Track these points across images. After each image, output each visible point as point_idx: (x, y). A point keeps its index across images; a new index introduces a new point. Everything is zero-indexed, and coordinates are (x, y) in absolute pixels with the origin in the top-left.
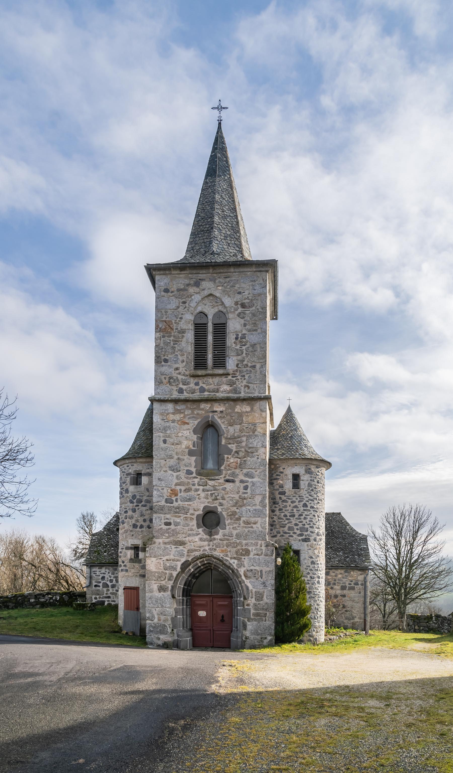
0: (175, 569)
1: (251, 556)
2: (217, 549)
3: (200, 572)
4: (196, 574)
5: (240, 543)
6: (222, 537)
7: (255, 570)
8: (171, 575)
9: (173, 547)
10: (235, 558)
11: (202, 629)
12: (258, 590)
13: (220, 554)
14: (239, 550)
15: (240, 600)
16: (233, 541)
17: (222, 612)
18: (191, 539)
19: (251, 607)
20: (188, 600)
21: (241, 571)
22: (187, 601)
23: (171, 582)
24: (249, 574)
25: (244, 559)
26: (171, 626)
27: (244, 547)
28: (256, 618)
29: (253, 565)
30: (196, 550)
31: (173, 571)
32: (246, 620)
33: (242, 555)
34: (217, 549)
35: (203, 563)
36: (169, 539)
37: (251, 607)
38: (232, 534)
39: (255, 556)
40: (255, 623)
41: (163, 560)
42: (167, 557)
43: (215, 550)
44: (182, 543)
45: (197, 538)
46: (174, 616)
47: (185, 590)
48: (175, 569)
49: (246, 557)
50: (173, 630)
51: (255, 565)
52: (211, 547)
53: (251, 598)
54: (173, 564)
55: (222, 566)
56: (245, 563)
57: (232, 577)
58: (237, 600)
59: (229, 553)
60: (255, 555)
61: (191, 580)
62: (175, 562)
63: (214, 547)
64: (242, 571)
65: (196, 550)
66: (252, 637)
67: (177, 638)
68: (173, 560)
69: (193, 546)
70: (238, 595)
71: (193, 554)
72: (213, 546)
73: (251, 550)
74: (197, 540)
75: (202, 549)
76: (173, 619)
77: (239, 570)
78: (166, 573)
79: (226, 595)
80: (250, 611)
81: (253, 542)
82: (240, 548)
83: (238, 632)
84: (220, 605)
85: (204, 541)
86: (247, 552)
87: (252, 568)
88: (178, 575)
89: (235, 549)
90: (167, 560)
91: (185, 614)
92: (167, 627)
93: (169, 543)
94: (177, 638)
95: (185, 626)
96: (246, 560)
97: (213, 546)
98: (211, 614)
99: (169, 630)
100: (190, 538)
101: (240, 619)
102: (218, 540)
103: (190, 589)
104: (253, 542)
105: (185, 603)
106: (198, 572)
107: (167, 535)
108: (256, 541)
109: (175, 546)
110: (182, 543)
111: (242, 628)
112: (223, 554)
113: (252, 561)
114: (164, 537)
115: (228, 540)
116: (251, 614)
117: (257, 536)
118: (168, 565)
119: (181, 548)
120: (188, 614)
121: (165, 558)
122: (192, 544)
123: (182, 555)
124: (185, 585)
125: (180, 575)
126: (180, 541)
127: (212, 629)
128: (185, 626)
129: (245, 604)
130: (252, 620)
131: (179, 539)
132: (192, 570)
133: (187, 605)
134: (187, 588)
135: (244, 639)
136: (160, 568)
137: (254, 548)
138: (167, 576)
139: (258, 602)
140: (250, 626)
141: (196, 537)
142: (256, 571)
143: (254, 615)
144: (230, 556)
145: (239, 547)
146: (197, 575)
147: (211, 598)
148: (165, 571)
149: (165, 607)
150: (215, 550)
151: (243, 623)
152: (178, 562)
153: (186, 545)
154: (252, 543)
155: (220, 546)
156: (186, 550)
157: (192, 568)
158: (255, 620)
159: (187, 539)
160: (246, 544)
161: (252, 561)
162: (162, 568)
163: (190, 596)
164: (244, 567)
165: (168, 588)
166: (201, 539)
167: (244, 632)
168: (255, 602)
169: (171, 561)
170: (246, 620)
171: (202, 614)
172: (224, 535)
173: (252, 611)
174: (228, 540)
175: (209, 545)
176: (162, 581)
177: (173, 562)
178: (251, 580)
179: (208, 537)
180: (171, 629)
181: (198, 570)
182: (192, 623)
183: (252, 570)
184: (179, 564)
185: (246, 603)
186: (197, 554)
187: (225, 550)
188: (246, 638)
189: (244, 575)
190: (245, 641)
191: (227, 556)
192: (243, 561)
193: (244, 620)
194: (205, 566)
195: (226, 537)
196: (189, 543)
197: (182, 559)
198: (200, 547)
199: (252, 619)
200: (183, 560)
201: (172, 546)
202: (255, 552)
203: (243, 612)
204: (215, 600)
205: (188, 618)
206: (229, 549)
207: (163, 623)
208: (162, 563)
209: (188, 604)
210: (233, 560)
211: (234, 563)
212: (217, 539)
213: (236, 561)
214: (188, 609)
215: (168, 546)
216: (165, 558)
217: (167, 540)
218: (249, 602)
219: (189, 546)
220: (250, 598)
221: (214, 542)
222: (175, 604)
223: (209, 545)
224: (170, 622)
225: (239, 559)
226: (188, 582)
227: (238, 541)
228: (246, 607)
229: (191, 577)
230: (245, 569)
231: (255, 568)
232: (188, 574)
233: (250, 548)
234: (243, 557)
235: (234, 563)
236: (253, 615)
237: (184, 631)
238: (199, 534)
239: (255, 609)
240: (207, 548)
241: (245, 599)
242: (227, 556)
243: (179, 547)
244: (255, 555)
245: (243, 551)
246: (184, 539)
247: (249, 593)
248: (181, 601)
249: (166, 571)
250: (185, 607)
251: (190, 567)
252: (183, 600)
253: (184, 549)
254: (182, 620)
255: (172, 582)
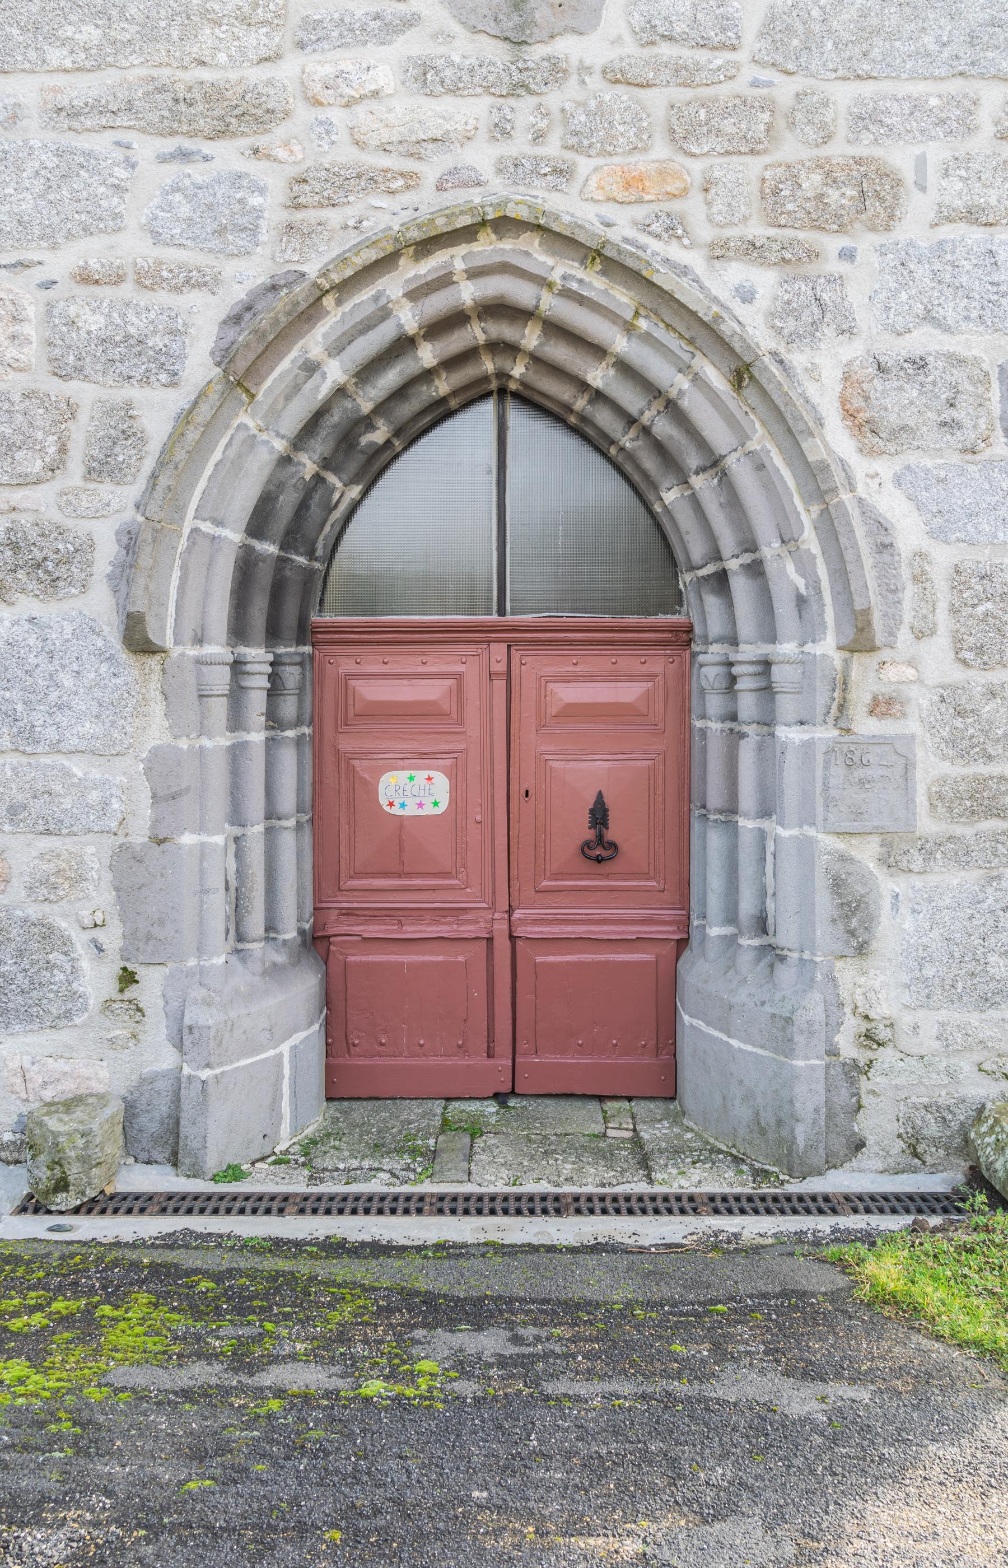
0: (166, 368)
1: (914, 226)
2: (584, 165)
3: (406, 410)
4: (367, 423)
5: (809, 110)
6: (630, 48)
7: (957, 361)
8: (123, 428)
9: (147, 148)
10: (752, 250)
11: (411, 931)
12: (983, 556)
13: (610, 211)
14: (792, 174)
15: (805, 663)
16: (741, 85)
17: (588, 772)
18: (329, 70)
19: (913, 726)
20: (291, 675)
21: (813, 371)
22: (274, 677)
23: (122, 499)
24: (896, 402)
25: (848, 255)
26: (112, 938)
27: (838, 150)
28: (968, 832)
29: (929, 317)
30: (371, 180)
31: (146, 381)
32: (866, 853)
33: (822, 218)
34: (584, 165)
35: (438, 304)
36: (110, 77)
37: (913, 726)
38: (726, 23)
39: (947, 232)
40: (954, 880)
41: (39, 275)
42: (90, 251)
43: (563, 172)
44: (243, 115)
45: (382, 66)
46: (139, 836)
47: (264, 576)
48: (166, 368)
49: (865, 243)
50: (128, 978)
51: (949, 313)
52: (519, 146)
53: (919, 635)
54: (143, 310)
55: (629, 329)
56: (856, 295)
57: (717, 434)
58: (766, 665)
59: (694, 208)
60: (946, 217)
61: (318, 479)
62: (163, 297)
63: (552, 148)
64: (819, 376)
65: (371, 180)
66: (929, 1021)
67: (166, 1059)
68: (149, 279)
69: (342, 136)
70: (784, 609)
71: (349, 214)
72: (539, 137)
73: (909, 176)
74: (384, 76)
75: (430, 172)
76: (135, 871)
77: (798, 359)
78: (72, 410)
79: (607, 619)
80: (908, 767)
81: (932, 93)
82: (806, 154)
83: (786, 974)
84: (573, 712)
85: (454, 91)
86: (875, 194)
87: (924, 340)
88: (185, 418)
89: (755, 165)
90: (86, 278)
91: (255, 804)
92: (66, 945)
93: (107, 112)
94: (166, 1059)
95: (256, 922)
96: (861, 272)
97: (539, 137)
98: (504, 788)
99: (96, 980)
100: (320, 66)
101: (806, 846)
102: (595, 82)
103: (309, 574)
104: (932, 93)
105: (257, 702)
106: (381, 408)
107: (90, 33)
108: (955, 86)
109: (169, 145)
110: (243, 115)
111: (826, 935)
112: (639, 212)
113: (922, 272)
114: (56, 56)
115: (685, 75)
116: (921, 799)
117: (973, 40)
118: (94, 322)
119: (228, 155)
120: (288, 799)
121: (60, 263)
122: (336, 115)
123: (238, 228)
124: (257, 527)
125: (205, 412)
126: (213, 94)
127: (501, 928)
128: (256, 922)
129: (860, 697)
130: (929, 856)
131: (205, 74)
132: (336, 372)
133: (274, 720)
134: (281, 561)
135: (848, 1049)
136: (11, 353)
137: (937, 152)
138: (80, 434)
139: (979, 679)
140: (908, 911)
141: (372, 53)
142: (958, 375)
143: (950, 800)
144: (705, 233)
145: (791, 149)
146: (379, 435)
147: (499, 651)
148: (55, 387)
149: (56, 748)
150: (563, 172)
151: (838, 885)
152: (193, 298)
153: (280, 131)
154: (917, 106)
155: (610, 138)
156: (275, 181)
157: (336, 349)
158: (961, 855)
159: (288, 70)
160: (866, 119)
161: (922, 272)
162: (32, 353)
163: (304, 633)
164: (848, 332)
165: (86, 547)
166: (424, 76)
167: (846, 973)
168: (958, 675)
169: (127, 290)
170: (866, 853)
171: (413, 791)
172: (651, 35)
173: (932, 767)
174: (685, 75)
175: (501, 131)
176: (25, 482)
177: (144, 299)
178: (911, 458)
179: (497, 52)
180: (112, 969)
181: (390, 378)
182: (325, 878)
183: (920, 364)
184: (204, 318)
185: (866, 680)
186: (387, 215)
187: (663, 173)
188: (870, 1039)
189: (849, 414)
190: (855, 1071)
191: (674, 229)
192: (837, 281)
193: (843, 858)
194: (456, 342)
195: (666, 50)
196: (304, 114)
197: (229, 268)
198: (415, 149)
199: (929, 849)
200: (245, 275)
201: (131, 137)
202: (954, 192)
203: (838, 771)
204: (533, 666)
205: (288, 843)
206: (697, 167)
207: (34, 911)
208: (31, 312)
209: (289, 707)
210: (737, 272)
211: (747, 296)
212: (584, 69)
213: (765, 281)
214: (288, 760)
215: (101, 143)
216: (60, 263)
217: (83, 88)
218: (891, 673)
219: (297, 143)
220: (904, 635)
221: (554, 99)
222: (157, 708)
223: (501, 131)
224: (100, 897)
225: (792, 260)
226: (287, 502)
227: (785, 90)
228: (866, 726)
229: (321, 446)
230: (852, 350)
231: (951, 344)
232: (295, 415)
233: (900, 158)
234: (832, 244)
235: (747, 299)
236: (936, 799)
237: (243, 978)
238: (410, 22)
239: (959, 747)
240: (481, 157)
241: (861, 640)
242: (674, 229)
243: (207, 148)
244: (946, 217)
245: (831, 179)
246: (256, 75)
247: (892, 591)
248: (220, 678)
249: (75, 388)
250: (257, 737)
251: (314, 342)
252: (237, 666)
253: (254, 168)
254: (220, 868)
255: (134, 491)
